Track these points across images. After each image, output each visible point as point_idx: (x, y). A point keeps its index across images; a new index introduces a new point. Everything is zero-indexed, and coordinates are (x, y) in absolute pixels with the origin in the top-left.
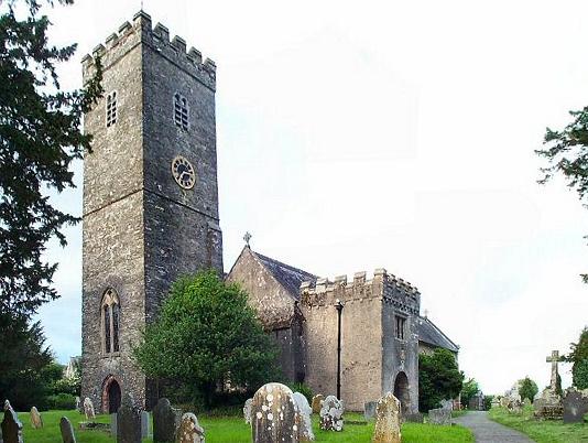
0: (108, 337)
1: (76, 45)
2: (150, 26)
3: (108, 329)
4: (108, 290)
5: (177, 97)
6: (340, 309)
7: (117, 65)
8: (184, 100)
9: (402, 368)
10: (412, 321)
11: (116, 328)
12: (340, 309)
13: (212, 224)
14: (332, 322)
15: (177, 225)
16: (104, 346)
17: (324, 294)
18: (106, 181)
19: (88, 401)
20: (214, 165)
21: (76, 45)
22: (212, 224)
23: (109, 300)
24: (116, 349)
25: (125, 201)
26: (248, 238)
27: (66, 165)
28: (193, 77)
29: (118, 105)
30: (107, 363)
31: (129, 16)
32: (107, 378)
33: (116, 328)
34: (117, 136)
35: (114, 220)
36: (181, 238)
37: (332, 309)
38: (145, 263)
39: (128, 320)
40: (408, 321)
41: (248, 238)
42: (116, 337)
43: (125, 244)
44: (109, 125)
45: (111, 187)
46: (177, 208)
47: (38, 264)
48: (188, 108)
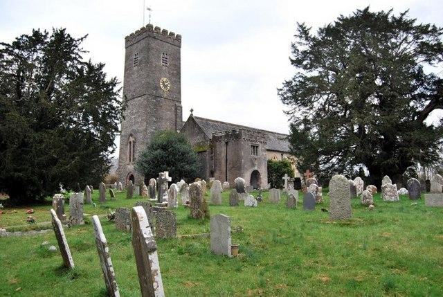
1: (415, 19)
3: (130, 152)
4: (131, 135)
6: (227, 143)
9: (256, 168)
11: (134, 151)
12: (227, 143)
13: (177, 104)
14: (224, 149)
17: (221, 137)
18: (132, 89)
20: (180, 78)
21: (415, 19)
22: (177, 104)
23: (132, 139)
24: (133, 161)
27: (112, 89)
30: (129, 167)
31: (48, 27)
34: (138, 71)
37: (224, 143)
40: (260, 148)
41: (192, 111)
43: (139, 116)
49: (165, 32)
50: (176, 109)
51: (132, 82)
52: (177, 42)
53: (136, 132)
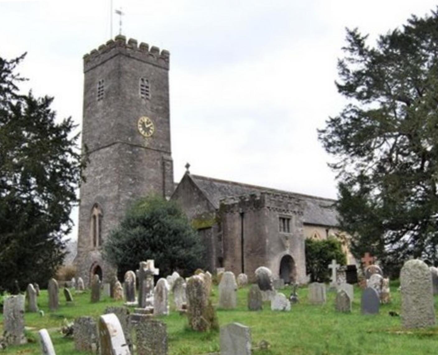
0: (95, 236)
2: (125, 42)
4: (96, 205)
5: (143, 80)
6: (242, 215)
7: (105, 64)
8: (147, 81)
9: (287, 252)
10: (297, 219)
12: (242, 215)
14: (238, 224)
15: (140, 161)
16: (92, 243)
18: (96, 134)
19: (81, 279)
20: (168, 117)
22: (166, 156)
23: (96, 212)
25: (108, 149)
26: (188, 166)
28: (154, 65)
29: (105, 88)
32: (93, 265)
33: (100, 230)
35: (100, 160)
36: (143, 169)
37: (237, 215)
38: (119, 189)
39: (107, 225)
41: (188, 166)
42: (100, 236)
43: (107, 176)
44: (99, 100)
45: (99, 139)
46: (141, 150)
47: (69, 201)
48: (150, 85)
49: (144, 46)
50: (163, 164)
51: (95, 124)
52: (162, 63)
53: (104, 200)
